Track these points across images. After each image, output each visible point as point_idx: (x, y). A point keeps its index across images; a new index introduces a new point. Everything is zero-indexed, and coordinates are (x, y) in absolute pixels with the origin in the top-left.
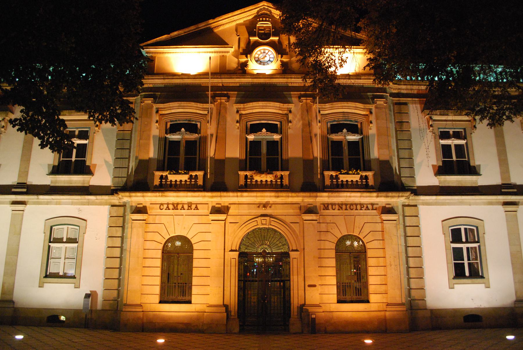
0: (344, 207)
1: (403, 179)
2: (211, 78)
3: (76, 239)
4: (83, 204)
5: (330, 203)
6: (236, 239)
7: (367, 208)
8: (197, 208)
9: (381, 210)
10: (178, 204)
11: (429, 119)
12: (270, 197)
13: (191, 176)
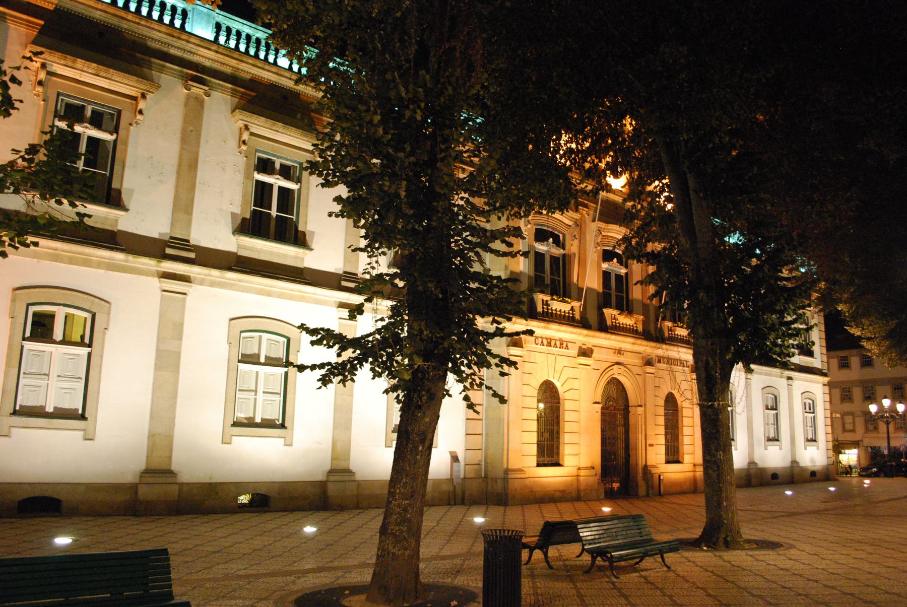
8: (567, 348)
11: (243, 129)
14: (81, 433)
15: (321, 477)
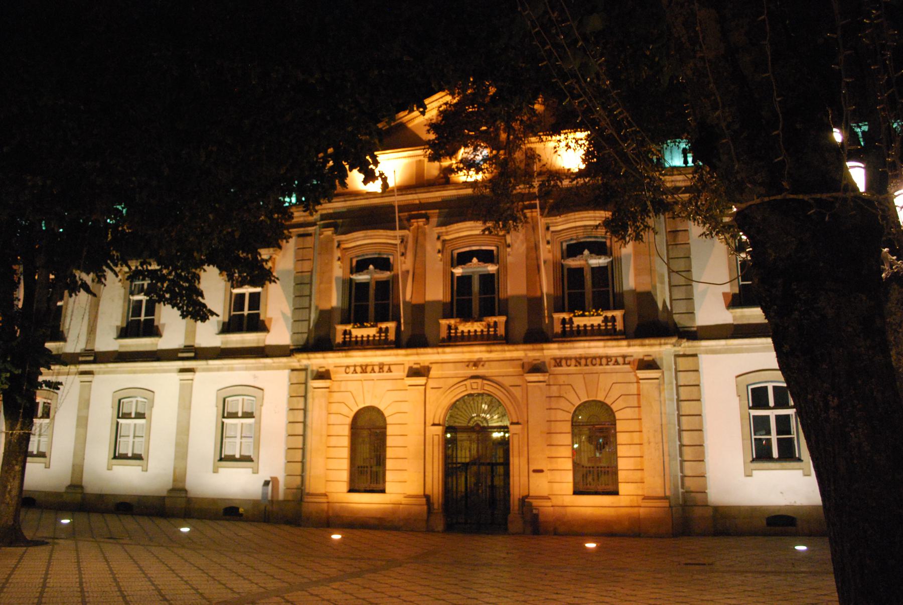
0: (583, 362)
1: (676, 318)
2: (398, 195)
3: (252, 413)
4: (258, 369)
5: (563, 357)
6: (440, 410)
7: (617, 363)
8: (390, 370)
9: (636, 364)
10: (367, 366)
12: (481, 352)
13: (381, 329)
14: (44, 465)
15: (165, 494)
